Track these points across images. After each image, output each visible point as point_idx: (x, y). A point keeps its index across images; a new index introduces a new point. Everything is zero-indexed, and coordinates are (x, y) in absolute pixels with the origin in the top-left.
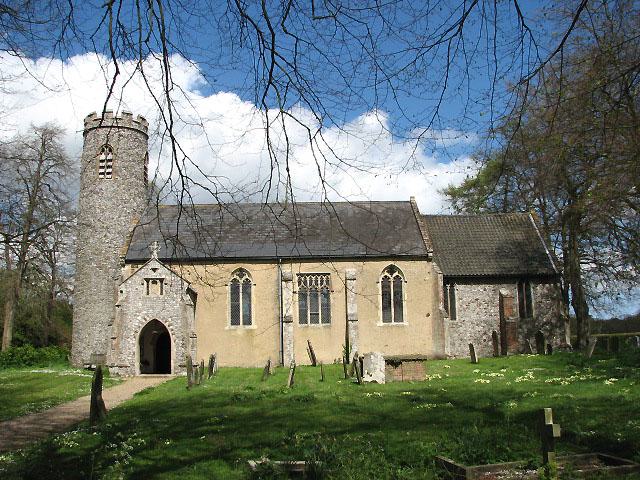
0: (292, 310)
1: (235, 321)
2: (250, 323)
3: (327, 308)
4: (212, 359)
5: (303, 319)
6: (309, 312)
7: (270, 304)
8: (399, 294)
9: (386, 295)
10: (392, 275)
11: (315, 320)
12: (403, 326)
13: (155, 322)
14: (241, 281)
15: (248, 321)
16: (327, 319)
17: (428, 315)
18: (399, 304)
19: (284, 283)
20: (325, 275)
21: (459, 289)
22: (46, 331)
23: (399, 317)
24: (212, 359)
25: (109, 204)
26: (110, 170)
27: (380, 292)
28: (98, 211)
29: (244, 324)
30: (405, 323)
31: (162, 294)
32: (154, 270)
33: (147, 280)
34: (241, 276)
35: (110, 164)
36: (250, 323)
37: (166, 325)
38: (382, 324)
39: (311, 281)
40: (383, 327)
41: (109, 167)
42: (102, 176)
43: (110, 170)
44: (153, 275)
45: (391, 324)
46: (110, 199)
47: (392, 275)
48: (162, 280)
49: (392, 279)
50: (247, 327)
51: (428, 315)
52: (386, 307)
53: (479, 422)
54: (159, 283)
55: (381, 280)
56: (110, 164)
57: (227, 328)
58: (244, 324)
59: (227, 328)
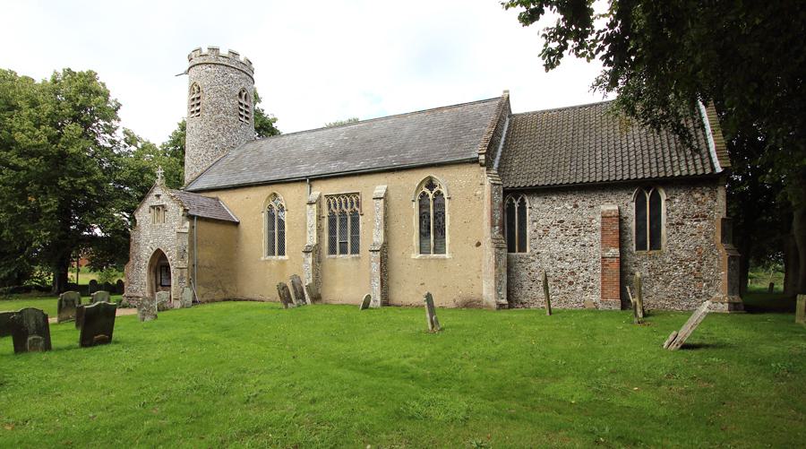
2: (284, 254)
4: (429, 297)
8: (440, 216)
9: (423, 217)
10: (431, 191)
11: (343, 251)
12: (445, 259)
13: (158, 250)
15: (282, 252)
16: (356, 250)
18: (440, 230)
20: (355, 194)
21: (534, 206)
23: (439, 249)
24: (429, 297)
26: (198, 108)
27: (446, 210)
30: (447, 255)
32: (158, 196)
36: (284, 254)
37: (167, 254)
40: (420, 259)
41: (198, 104)
44: (156, 202)
45: (428, 256)
47: (431, 191)
48: (163, 206)
49: (431, 196)
50: (280, 257)
52: (424, 234)
53: (740, 444)
55: (418, 198)
57: (263, 258)
58: (279, 254)
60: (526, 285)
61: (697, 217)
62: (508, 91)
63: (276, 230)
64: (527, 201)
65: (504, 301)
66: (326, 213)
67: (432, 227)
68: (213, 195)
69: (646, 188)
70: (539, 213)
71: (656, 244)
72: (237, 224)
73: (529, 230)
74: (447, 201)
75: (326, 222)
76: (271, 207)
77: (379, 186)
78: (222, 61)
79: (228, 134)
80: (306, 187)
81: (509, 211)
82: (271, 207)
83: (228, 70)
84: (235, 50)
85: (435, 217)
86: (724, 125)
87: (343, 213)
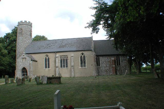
0: (58, 64)
1: (46, 67)
3: (67, 65)
5: (61, 67)
6: (63, 65)
7: (53, 63)
11: (64, 67)
14: (83, 56)
15: (49, 67)
16: (67, 67)
17: (92, 65)
18: (85, 62)
19: (56, 58)
21: (101, 58)
22: (10, 71)
25: (21, 41)
26: (21, 34)
28: (127, 102)
29: (63, 67)
30: (86, 67)
31: (23, 61)
32: (24, 56)
33: (22, 58)
34: (47, 56)
35: (22, 33)
37: (26, 68)
38: (80, 67)
39: (63, 57)
41: (21, 33)
42: (20, 36)
43: (21, 34)
44: (23, 57)
46: (22, 40)
48: (25, 58)
49: (83, 56)
51: (92, 65)
52: (82, 63)
54: (25, 59)
56: (22, 33)
57: (44, 69)
59: (44, 69)
60: (100, 72)
61: (125, 60)
62: (97, 33)
63: (47, 63)
64: (100, 57)
65: (97, 75)
66: (60, 59)
67: (83, 61)
68: (30, 55)
69: (118, 55)
70: (102, 59)
71: (120, 64)
72: (37, 61)
73: (100, 62)
74: (86, 57)
75: (60, 60)
76: (46, 58)
77: (72, 54)
78: (27, 24)
79: (28, 40)
80: (54, 54)
81: (97, 59)
82: (46, 58)
83: (28, 26)
84: (26, 20)
85: (84, 60)
86: (3, 85)
87: (64, 59)
